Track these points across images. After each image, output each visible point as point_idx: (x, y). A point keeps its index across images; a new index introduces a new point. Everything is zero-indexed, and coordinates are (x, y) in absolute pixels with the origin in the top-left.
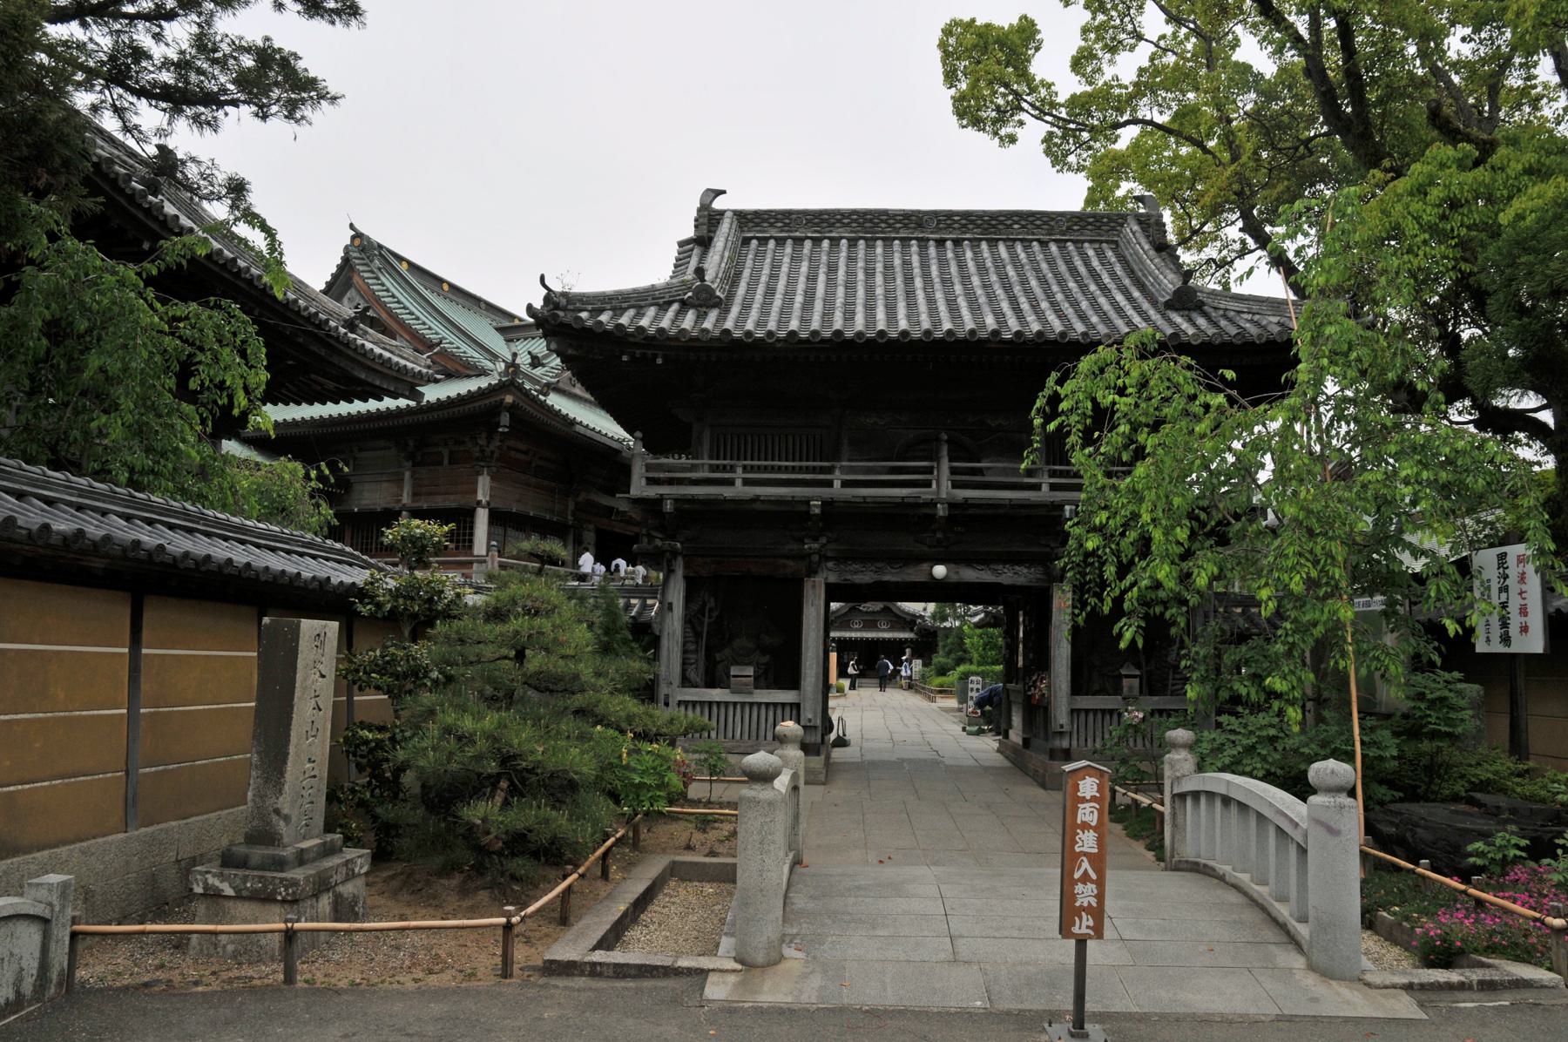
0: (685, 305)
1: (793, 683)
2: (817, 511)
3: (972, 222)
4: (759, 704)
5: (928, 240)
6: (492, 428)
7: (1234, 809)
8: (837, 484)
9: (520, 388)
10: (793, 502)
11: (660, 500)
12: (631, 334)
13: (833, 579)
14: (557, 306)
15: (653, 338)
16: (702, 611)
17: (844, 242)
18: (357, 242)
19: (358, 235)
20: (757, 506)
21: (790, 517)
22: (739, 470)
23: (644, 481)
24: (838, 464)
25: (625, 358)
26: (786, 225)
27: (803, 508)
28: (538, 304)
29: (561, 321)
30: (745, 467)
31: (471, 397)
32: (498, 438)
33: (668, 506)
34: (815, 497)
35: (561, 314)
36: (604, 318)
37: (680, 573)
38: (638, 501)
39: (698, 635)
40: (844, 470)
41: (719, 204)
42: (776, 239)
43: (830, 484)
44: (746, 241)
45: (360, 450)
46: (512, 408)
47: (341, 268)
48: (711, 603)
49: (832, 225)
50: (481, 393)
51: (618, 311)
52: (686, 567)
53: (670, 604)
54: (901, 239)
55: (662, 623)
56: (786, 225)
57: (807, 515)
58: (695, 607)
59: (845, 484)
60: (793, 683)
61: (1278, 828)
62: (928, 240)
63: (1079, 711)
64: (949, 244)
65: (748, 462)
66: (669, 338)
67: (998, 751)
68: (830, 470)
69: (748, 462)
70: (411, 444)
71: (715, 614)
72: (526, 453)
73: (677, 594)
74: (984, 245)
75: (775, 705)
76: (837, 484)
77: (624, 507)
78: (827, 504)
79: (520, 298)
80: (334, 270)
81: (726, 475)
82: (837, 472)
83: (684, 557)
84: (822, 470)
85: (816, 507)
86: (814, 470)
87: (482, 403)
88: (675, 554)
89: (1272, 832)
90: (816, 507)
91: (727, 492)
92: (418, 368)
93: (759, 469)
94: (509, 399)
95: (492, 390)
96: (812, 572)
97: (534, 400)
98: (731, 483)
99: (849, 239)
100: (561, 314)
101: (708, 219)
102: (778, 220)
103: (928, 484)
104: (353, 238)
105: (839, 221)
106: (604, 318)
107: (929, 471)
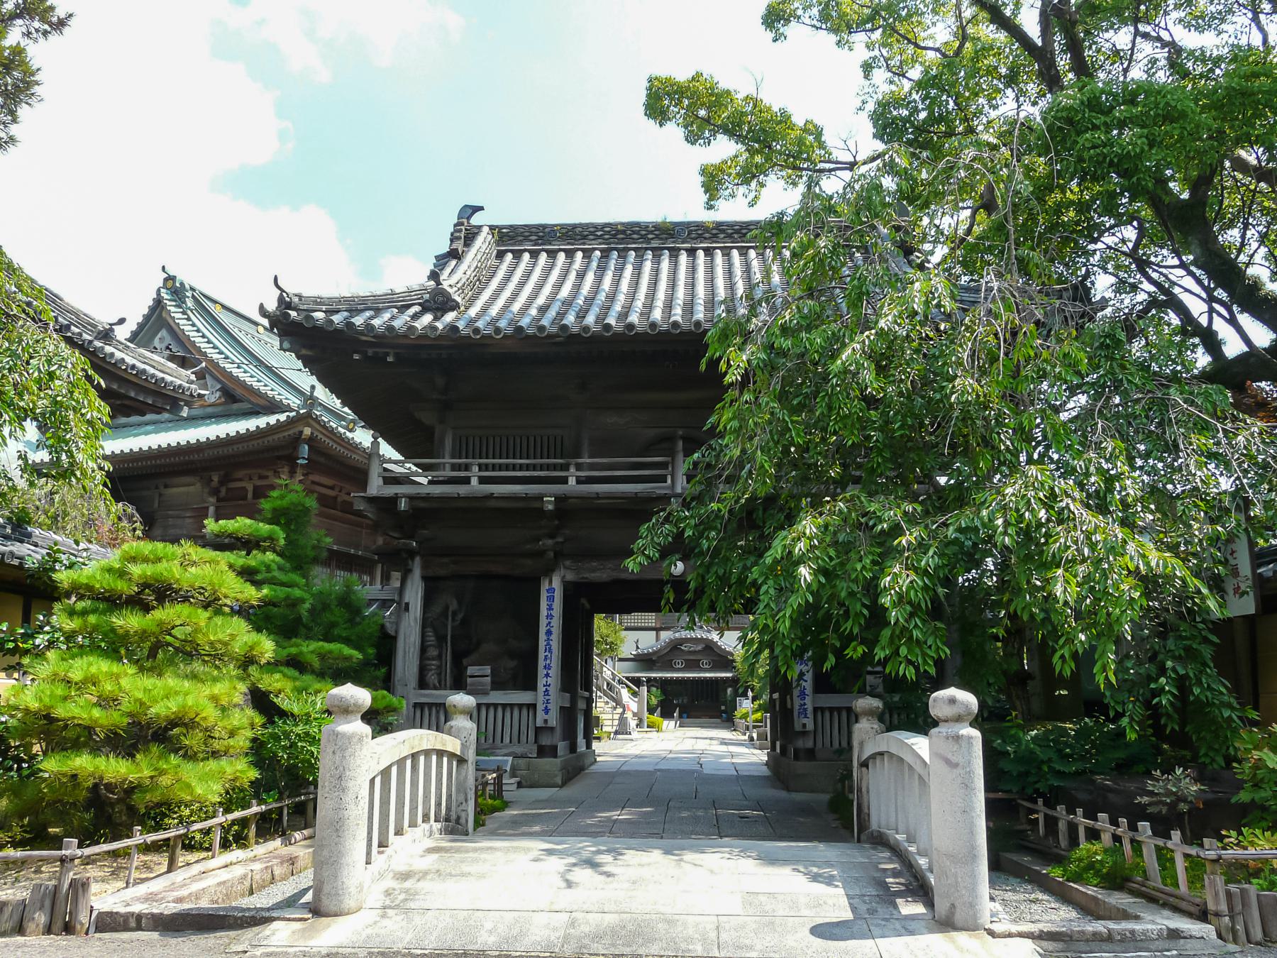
0: (425, 309)
1: (531, 685)
2: (550, 507)
3: (723, 231)
4: (496, 706)
5: (679, 249)
6: (291, 460)
7: (878, 758)
8: (572, 481)
9: (317, 420)
10: (527, 498)
11: (394, 500)
12: (361, 333)
13: (570, 577)
14: (289, 306)
15: (382, 336)
16: (445, 613)
17: (598, 253)
18: (170, 284)
19: (170, 279)
20: (492, 504)
21: (526, 511)
22: (476, 469)
23: (381, 481)
24: (574, 461)
25: (356, 357)
26: (540, 238)
27: (537, 505)
28: (272, 306)
29: (296, 327)
30: (480, 466)
31: (270, 430)
32: (299, 471)
33: (403, 505)
34: (549, 495)
35: (293, 314)
36: (337, 318)
37: (417, 573)
38: (372, 500)
39: (441, 639)
40: (579, 467)
41: (476, 220)
42: (530, 251)
43: (564, 481)
44: (500, 255)
45: (166, 486)
46: (311, 441)
47: (153, 310)
48: (454, 605)
49: (585, 237)
50: (279, 426)
51: (354, 311)
52: (425, 567)
53: (407, 604)
54: (653, 249)
55: (397, 624)
56: (540, 238)
57: (541, 512)
58: (437, 609)
59: (579, 481)
60: (531, 685)
61: (920, 776)
62: (679, 249)
63: (822, 709)
64: (701, 253)
65: (481, 461)
66: (398, 336)
67: (767, 764)
68: (565, 467)
69: (481, 461)
70: (216, 479)
71: (460, 616)
72: (332, 488)
73: (415, 594)
74: (735, 253)
75: (512, 705)
76: (572, 481)
77: (360, 506)
78: (560, 499)
79: (250, 295)
80: (146, 311)
81: (463, 474)
82: (572, 470)
83: (422, 557)
84: (555, 467)
85: (549, 503)
86: (548, 467)
87: (281, 435)
88: (412, 554)
89: (916, 777)
90: (549, 503)
91: (462, 490)
92: (178, 382)
93: (494, 467)
94: (307, 431)
95: (290, 422)
96: (548, 572)
97: (340, 436)
98: (467, 481)
99: (602, 251)
100: (293, 314)
101: (465, 234)
102: (532, 234)
103: (662, 479)
104: (166, 280)
105: (592, 233)
106: (337, 318)
107: (663, 465)
